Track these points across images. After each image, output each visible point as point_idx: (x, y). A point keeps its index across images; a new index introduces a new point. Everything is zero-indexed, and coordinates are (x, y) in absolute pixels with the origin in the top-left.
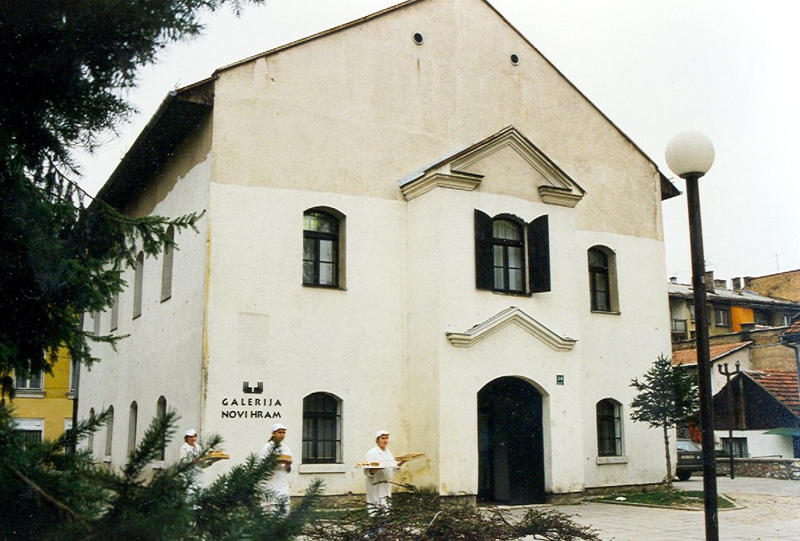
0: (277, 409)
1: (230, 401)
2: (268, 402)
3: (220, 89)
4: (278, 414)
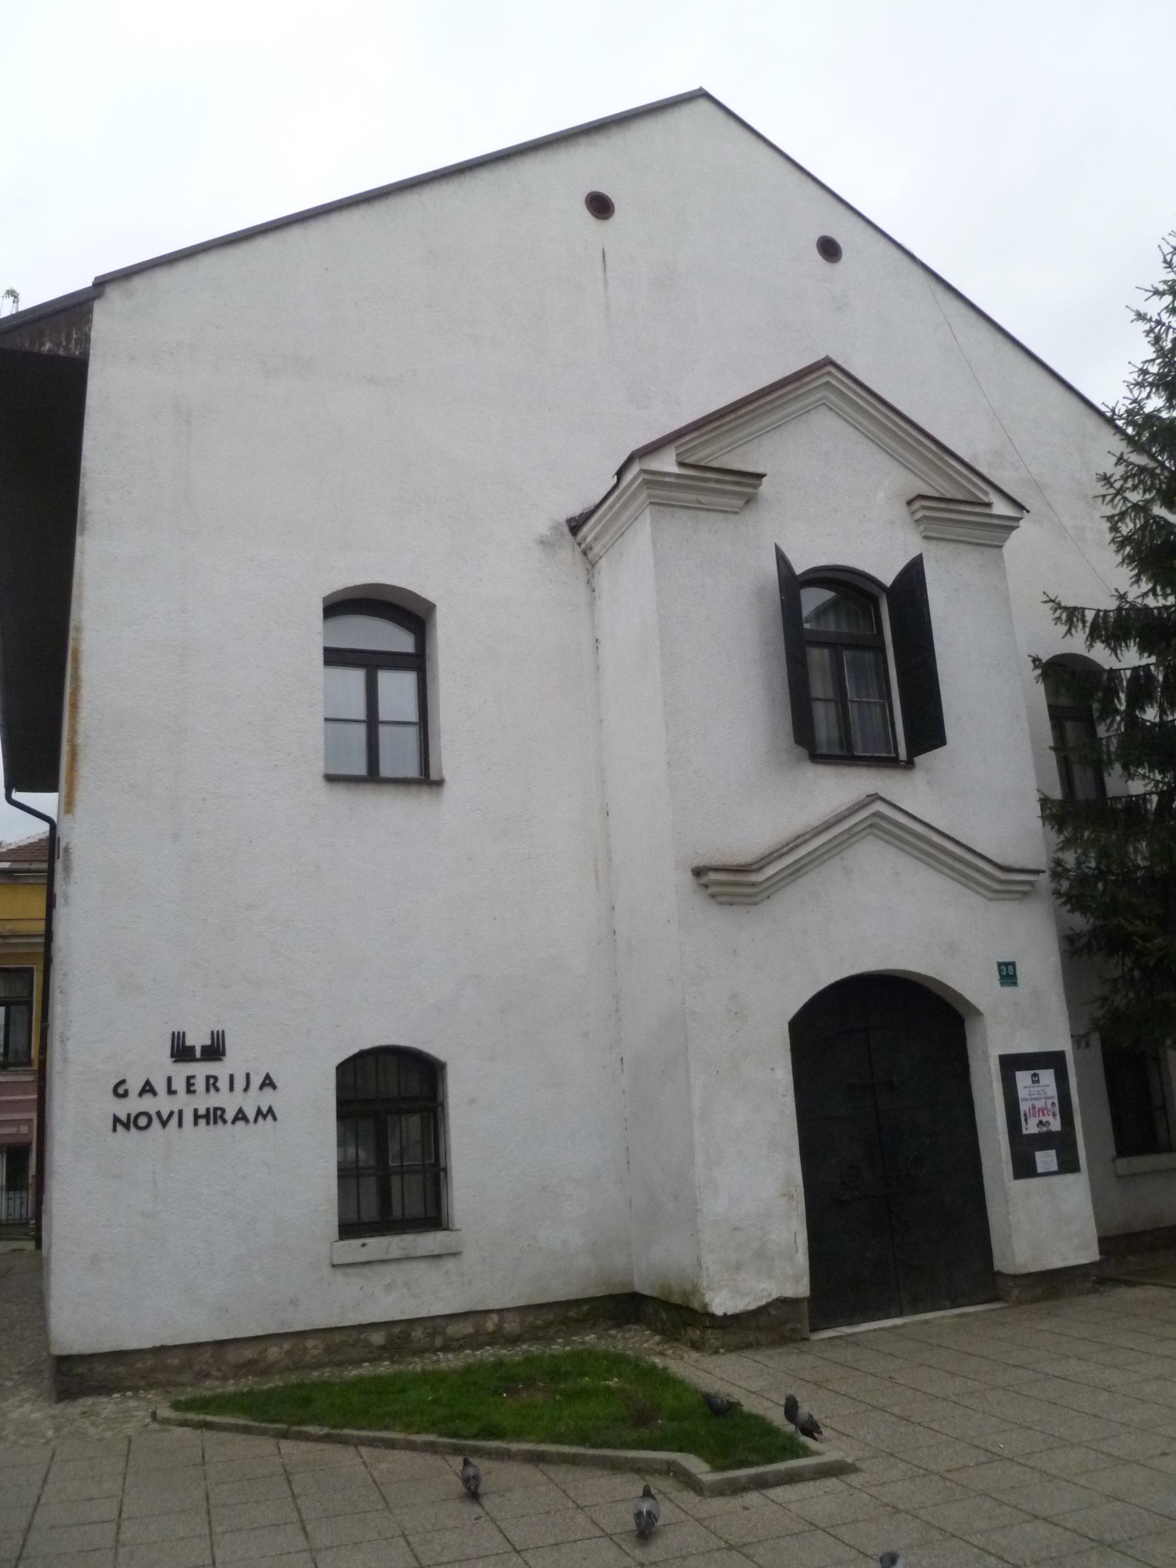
0: (266, 1099)
1: (135, 1086)
2: (240, 1083)
3: (104, 323)
4: (270, 1110)
